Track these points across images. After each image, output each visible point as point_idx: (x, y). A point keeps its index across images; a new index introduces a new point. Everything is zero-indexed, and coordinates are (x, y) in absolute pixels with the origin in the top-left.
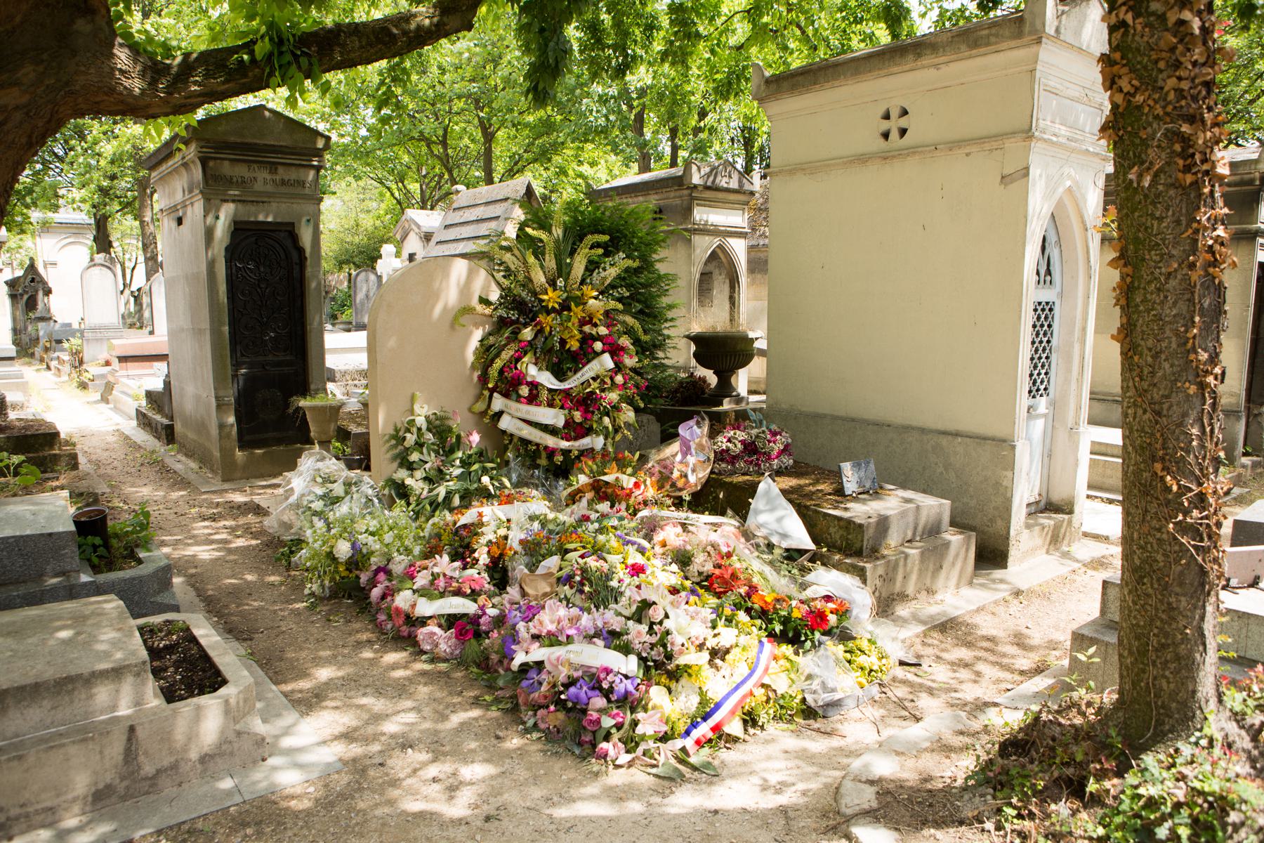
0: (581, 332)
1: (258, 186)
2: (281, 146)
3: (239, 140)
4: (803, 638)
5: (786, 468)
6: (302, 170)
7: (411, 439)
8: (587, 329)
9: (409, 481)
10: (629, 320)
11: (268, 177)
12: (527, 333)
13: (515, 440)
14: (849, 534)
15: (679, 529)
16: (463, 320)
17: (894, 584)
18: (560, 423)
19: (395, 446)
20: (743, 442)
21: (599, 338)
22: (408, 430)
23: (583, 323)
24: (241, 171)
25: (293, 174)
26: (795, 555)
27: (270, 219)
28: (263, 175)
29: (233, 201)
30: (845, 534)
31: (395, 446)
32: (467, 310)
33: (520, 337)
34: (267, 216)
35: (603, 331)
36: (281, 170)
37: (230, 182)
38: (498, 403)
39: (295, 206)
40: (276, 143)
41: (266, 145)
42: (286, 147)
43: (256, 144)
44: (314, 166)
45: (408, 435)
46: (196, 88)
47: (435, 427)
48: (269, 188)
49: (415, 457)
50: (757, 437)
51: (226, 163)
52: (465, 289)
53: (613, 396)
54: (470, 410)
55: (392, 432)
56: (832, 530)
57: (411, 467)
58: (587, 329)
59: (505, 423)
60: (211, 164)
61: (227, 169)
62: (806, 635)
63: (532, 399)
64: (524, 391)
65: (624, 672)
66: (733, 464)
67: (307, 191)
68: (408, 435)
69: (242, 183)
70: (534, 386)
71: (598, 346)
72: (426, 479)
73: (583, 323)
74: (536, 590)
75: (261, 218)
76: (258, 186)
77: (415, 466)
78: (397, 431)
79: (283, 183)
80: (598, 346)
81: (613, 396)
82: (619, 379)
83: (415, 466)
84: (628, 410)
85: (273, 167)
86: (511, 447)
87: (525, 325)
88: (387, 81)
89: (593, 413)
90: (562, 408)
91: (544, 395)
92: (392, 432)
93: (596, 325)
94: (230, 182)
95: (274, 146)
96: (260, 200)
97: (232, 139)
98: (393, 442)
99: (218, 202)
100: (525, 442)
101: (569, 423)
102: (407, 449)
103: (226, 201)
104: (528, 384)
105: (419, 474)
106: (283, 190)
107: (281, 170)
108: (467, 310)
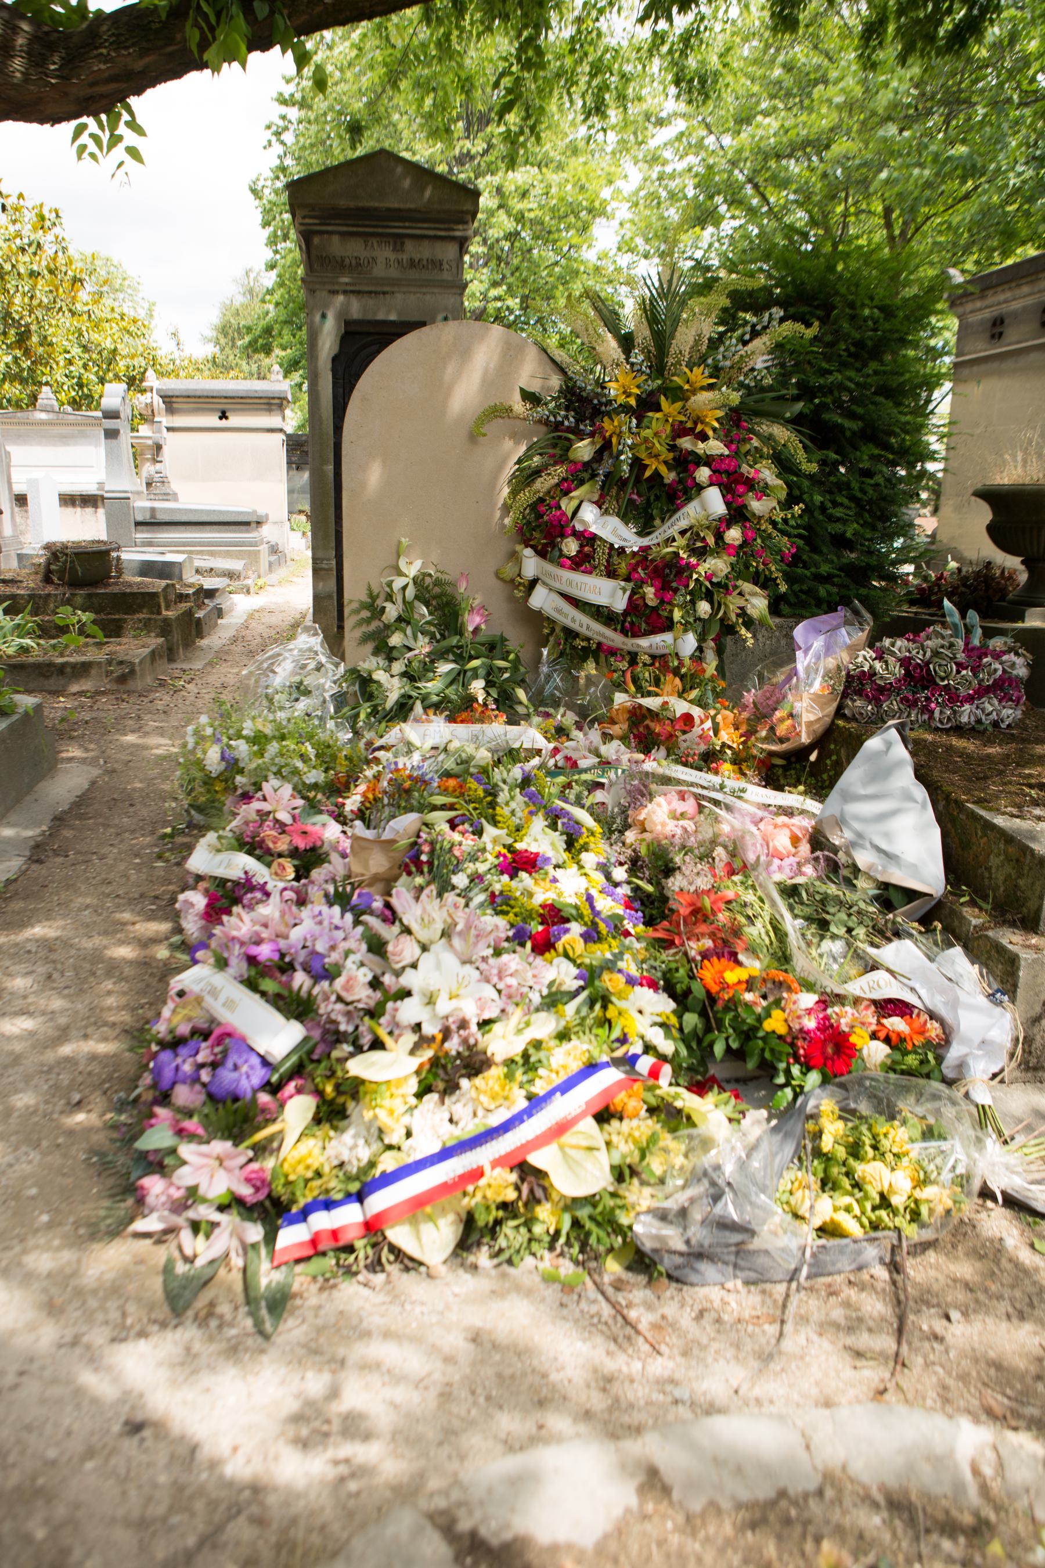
0: (673, 448)
1: (379, 271)
2: (410, 210)
3: (352, 204)
4: (781, 1080)
5: (995, 724)
6: (438, 245)
7: (392, 612)
8: (686, 443)
9: (380, 676)
10: (781, 433)
11: (392, 256)
12: (583, 449)
13: (558, 630)
14: (1020, 875)
15: (689, 806)
16: (489, 428)
17: (609, 1093)
18: (620, 604)
19: (368, 621)
20: (905, 662)
21: (708, 461)
22: (389, 598)
23: (680, 431)
24: (354, 249)
25: (424, 251)
26: (895, 898)
27: (393, 317)
28: (384, 254)
29: (345, 292)
30: (1013, 873)
31: (368, 621)
32: (499, 412)
33: (572, 455)
34: (388, 312)
35: (715, 447)
36: (409, 245)
37: (340, 265)
38: (531, 564)
39: (428, 297)
40: (402, 206)
41: (389, 209)
42: (415, 211)
43: (376, 209)
44: (453, 239)
45: (389, 606)
46: (102, 67)
47: (435, 597)
48: (394, 273)
49: (396, 640)
50: (936, 653)
51: (336, 239)
52: (491, 382)
53: (717, 566)
54: (497, 575)
55: (365, 598)
56: (994, 861)
57: (390, 655)
58: (686, 443)
59: (540, 599)
60: (316, 240)
61: (337, 247)
62: (788, 1072)
63: (581, 562)
64: (571, 547)
65: (496, 1028)
66: (878, 704)
67: (446, 276)
68: (389, 606)
69: (357, 267)
70: (588, 539)
71: (703, 474)
72: (404, 674)
73: (680, 431)
74: (366, 866)
75: (381, 316)
76: (379, 271)
77: (395, 654)
78: (373, 597)
79: (413, 264)
80: (703, 474)
81: (717, 566)
82: (734, 535)
83: (395, 654)
84: (754, 594)
85: (398, 241)
86: (552, 639)
87: (581, 436)
88: (514, 69)
89: (676, 590)
90: (627, 579)
91: (601, 556)
92: (365, 598)
93: (703, 437)
94: (340, 265)
95: (399, 210)
96: (378, 291)
97: (343, 203)
98: (365, 614)
99: (324, 294)
100: (570, 634)
101: (635, 606)
102: (387, 627)
103: (335, 292)
104: (577, 535)
105: (398, 667)
106: (413, 274)
107: (409, 245)
108: (499, 412)
